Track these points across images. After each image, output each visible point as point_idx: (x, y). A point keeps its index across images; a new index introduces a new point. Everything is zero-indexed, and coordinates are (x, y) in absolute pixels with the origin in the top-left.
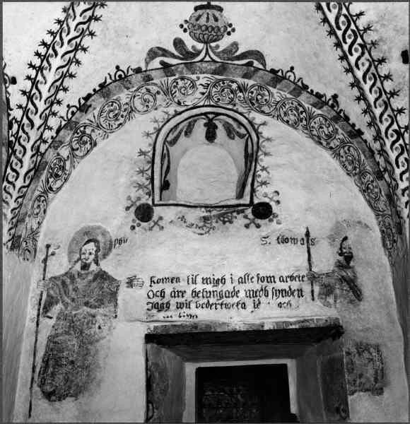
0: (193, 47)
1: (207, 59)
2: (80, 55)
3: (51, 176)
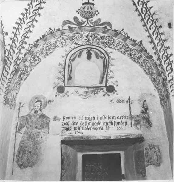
0: (82, 20)
1: (88, 25)
2: (34, 23)
3: (22, 74)
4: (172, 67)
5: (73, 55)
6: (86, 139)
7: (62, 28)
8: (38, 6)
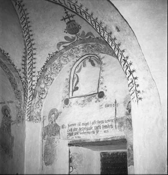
0: (72, 37)
1: (78, 39)
3: (40, 94)
4: (130, 69)
5: (76, 67)
6: (83, 142)
7: (59, 50)
8: (30, 44)
